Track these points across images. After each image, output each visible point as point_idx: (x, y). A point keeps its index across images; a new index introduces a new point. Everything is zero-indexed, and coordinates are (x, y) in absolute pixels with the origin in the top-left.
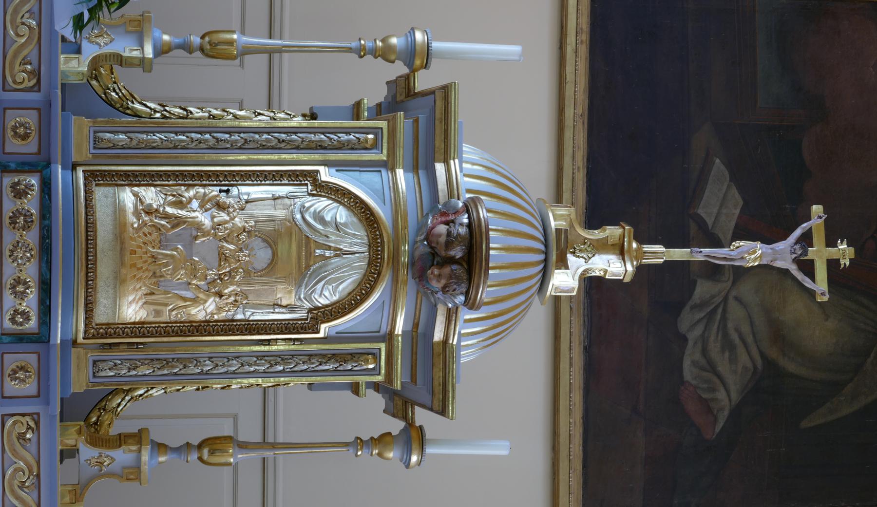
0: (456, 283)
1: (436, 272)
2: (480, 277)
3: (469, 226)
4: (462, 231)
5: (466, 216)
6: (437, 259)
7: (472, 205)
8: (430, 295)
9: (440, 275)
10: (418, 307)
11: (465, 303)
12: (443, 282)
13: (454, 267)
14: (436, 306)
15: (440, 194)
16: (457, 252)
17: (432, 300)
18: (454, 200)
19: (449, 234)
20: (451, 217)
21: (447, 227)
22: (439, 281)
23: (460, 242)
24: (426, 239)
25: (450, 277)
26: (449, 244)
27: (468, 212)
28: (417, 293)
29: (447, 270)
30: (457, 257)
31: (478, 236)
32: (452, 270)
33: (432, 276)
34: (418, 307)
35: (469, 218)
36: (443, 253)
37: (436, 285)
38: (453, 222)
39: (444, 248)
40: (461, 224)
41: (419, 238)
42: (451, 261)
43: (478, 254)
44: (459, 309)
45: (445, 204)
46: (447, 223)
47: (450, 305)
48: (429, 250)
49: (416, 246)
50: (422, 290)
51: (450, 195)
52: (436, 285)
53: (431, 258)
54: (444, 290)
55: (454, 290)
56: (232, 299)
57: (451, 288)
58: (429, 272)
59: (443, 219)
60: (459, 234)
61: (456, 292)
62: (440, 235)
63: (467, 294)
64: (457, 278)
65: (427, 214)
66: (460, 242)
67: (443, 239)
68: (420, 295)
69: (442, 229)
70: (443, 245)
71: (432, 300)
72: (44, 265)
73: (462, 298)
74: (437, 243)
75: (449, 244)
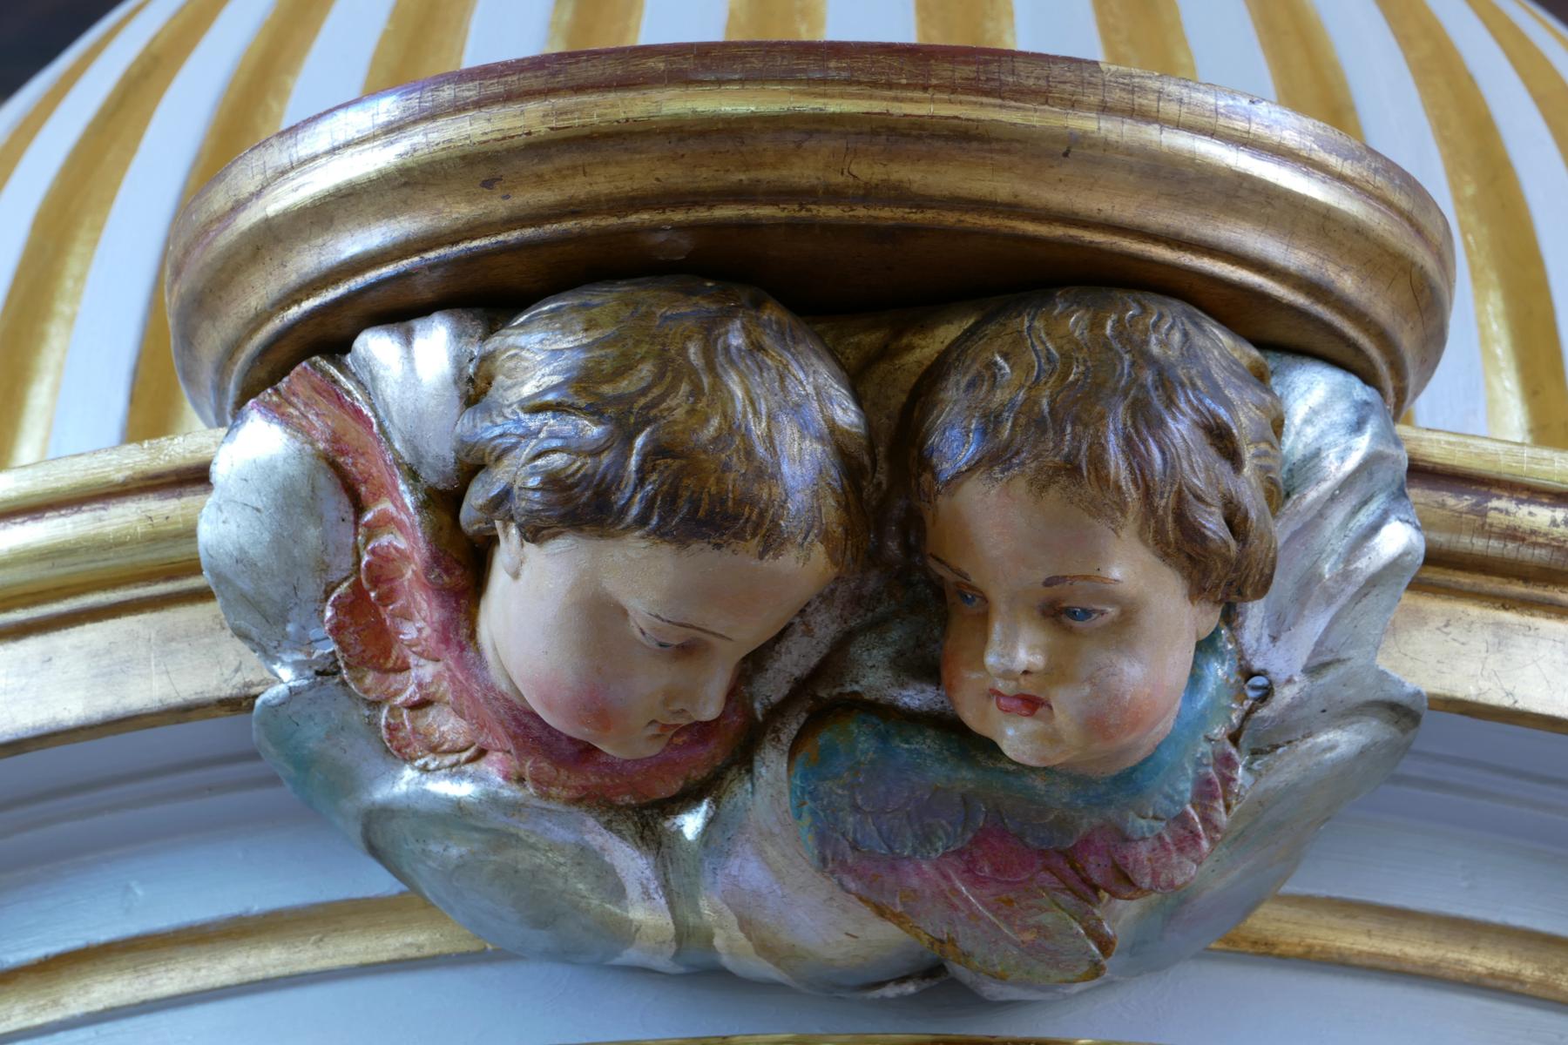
0: (1145, 418)
1: (1018, 650)
2: (1070, 149)
3: (486, 294)
4: (539, 354)
5: (376, 346)
6: (873, 676)
7: (260, 289)
8: (1286, 769)
9: (1061, 612)
10: (1415, 948)
11: (1386, 365)
12: (1128, 566)
13: (955, 443)
14: (1403, 713)
15: (147, 689)
16: (792, 416)
17: (1342, 740)
18: (220, 526)
19: (578, 507)
20: (402, 531)
21: (509, 547)
22: (1127, 621)
23: (670, 369)
24: (646, 819)
25: (1076, 473)
26: (700, 503)
27: (327, 338)
28: (1267, 953)
29: (992, 521)
30: (846, 415)
31: (603, 181)
32: (994, 459)
33: (1066, 704)
34: (1415, 948)
35: (398, 310)
36: (803, 567)
37: (1160, 665)
38: (444, 501)
39: (741, 559)
40: (474, 389)
41: (647, 914)
42: (886, 485)
43: (804, 171)
44: (1440, 449)
45: (263, 624)
46: (465, 567)
47: (1397, 539)
48: (772, 766)
49: (730, 945)
50: (1204, 873)
51: (163, 578)
52: (1160, 665)
53: (862, 741)
54: (1225, 570)
55: (1221, 439)
56: (1028, 937)
57: (1199, 467)
58: (1015, 738)
59: (418, 620)
60: (583, 391)
61: (1244, 419)
62: (597, 618)
63: (1281, 332)
64: (1080, 402)
65: (380, 834)
66: (670, 369)
67: (642, 575)
68: (1270, 921)
69: (529, 602)
70: (704, 559)
71: (1342, 740)
72: (1541, 555)
73: (1314, 397)
74: (688, 649)
75: (700, 503)
